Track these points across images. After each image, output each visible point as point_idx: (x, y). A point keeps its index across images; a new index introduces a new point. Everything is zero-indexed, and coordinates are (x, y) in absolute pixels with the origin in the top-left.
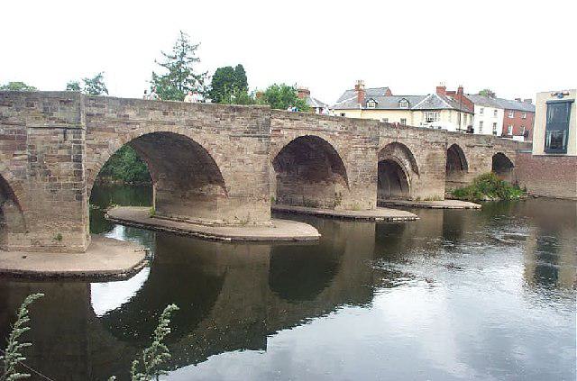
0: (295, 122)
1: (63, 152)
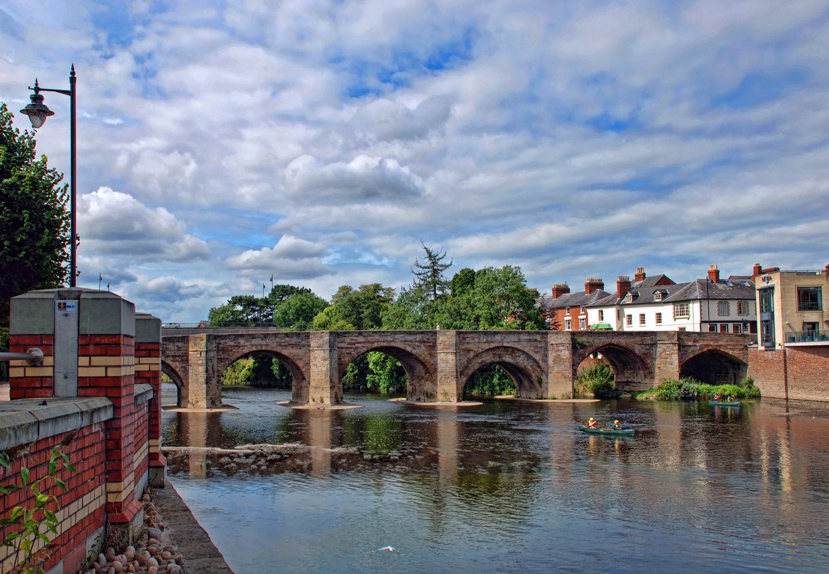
0: (369, 338)
1: (200, 362)
